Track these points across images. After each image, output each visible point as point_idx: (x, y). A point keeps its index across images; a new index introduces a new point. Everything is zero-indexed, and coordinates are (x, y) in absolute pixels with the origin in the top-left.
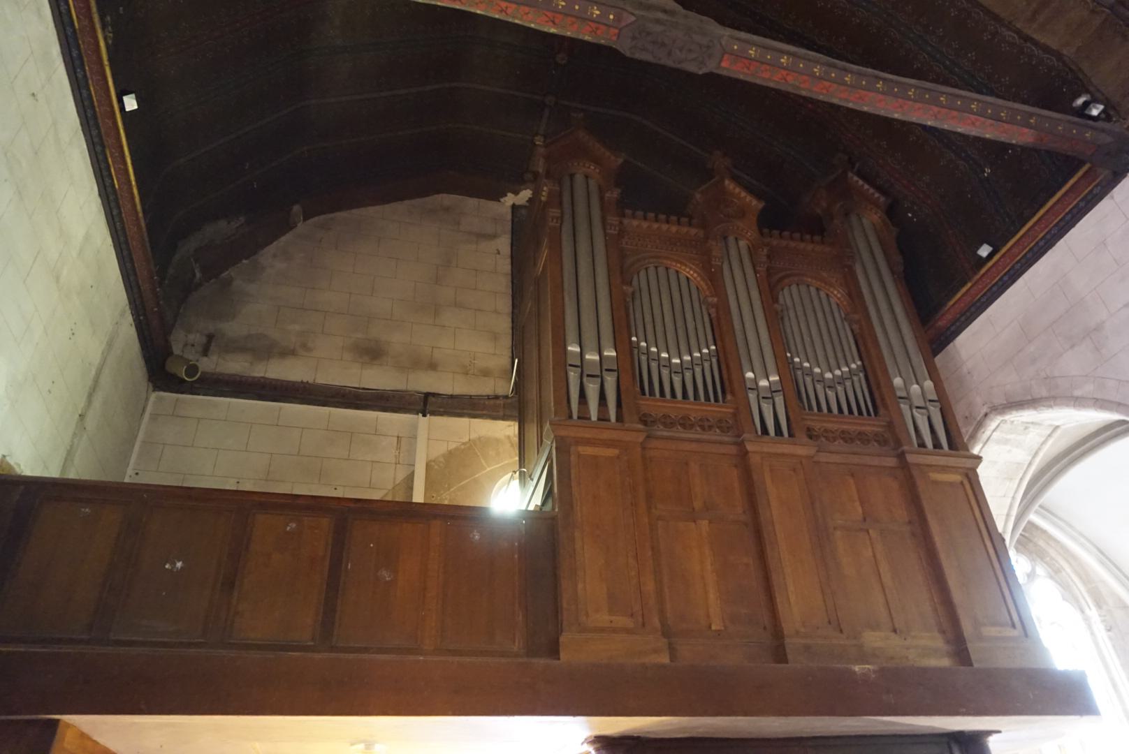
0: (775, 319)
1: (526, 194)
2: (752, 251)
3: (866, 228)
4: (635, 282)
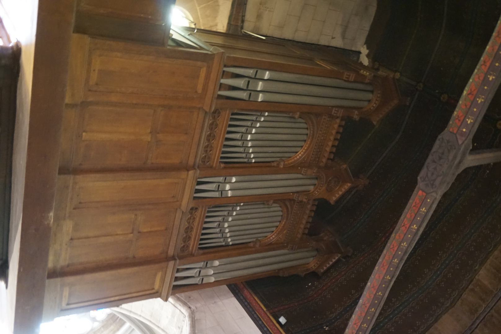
0: (263, 200)
1: (365, 61)
2: (306, 192)
3: (307, 259)
4: (300, 120)
